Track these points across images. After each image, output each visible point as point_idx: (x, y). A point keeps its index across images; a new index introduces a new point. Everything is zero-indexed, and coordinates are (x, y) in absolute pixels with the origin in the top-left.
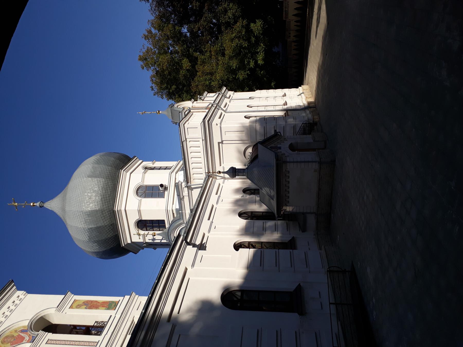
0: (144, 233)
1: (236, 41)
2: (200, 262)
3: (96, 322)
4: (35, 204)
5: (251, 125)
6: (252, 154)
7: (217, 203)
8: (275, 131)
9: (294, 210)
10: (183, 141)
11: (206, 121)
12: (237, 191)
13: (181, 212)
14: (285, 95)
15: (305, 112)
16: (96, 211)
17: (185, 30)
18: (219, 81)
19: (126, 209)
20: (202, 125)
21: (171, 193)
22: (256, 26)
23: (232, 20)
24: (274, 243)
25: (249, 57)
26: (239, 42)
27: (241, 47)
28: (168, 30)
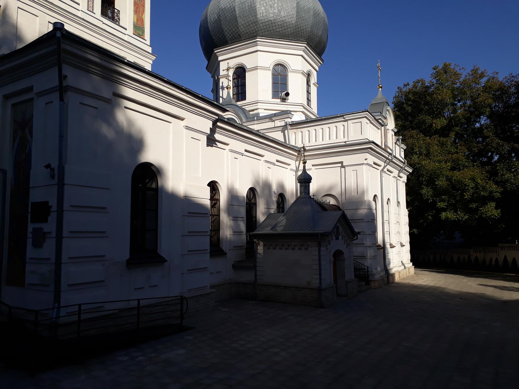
0: (230, 75)
1: (472, 185)
2: (192, 138)
3: (119, 11)
5: (366, 202)
6: (328, 205)
7: (267, 161)
8: (359, 233)
9: (258, 255)
10: (344, 116)
11: (371, 145)
12: (281, 186)
13: (255, 119)
14: (402, 246)
15: (381, 271)
16: (256, 15)
17: (484, 120)
18: (418, 164)
19: (258, 52)
20: (365, 140)
21: (279, 106)
22: (492, 209)
23: (500, 179)
24: (219, 230)
25: (451, 201)
26: (471, 188)
27: (464, 191)
28: (486, 99)
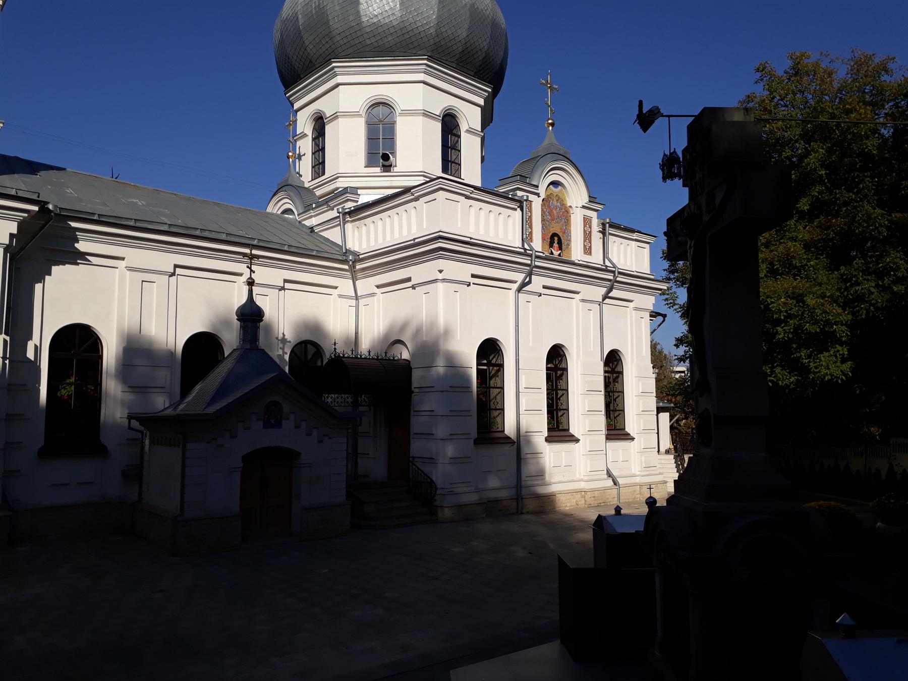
6: (386, 360)
10: (412, 191)
11: (440, 242)
19: (340, 86)
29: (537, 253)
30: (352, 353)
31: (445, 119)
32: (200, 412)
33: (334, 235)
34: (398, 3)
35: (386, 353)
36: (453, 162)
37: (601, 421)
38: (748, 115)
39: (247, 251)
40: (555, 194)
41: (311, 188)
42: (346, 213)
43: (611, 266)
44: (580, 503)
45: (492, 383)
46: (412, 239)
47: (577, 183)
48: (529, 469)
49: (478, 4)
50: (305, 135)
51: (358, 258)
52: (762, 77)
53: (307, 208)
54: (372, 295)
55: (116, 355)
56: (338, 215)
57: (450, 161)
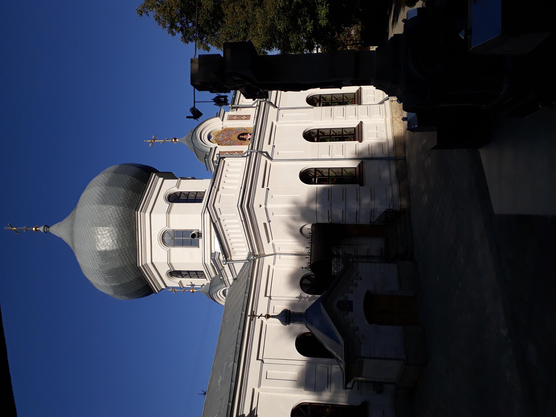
4: (38, 229)
6: (312, 238)
10: (214, 222)
11: (244, 207)
19: (153, 262)
29: (250, 149)
30: (308, 258)
31: (171, 201)
32: (343, 348)
33: (238, 267)
34: (105, 228)
35: (308, 238)
36: (196, 196)
37: (350, 108)
38: (194, 61)
39: (248, 318)
40: (215, 137)
41: (210, 280)
42: (226, 260)
43: (257, 103)
44: (399, 121)
45: (326, 175)
46: (241, 222)
47: (209, 125)
48: (378, 153)
49: (105, 181)
50: (180, 282)
51: (252, 253)
52: (145, 12)
53: (223, 281)
54: (273, 245)
55: (308, 395)
56: (227, 264)
57: (195, 198)
